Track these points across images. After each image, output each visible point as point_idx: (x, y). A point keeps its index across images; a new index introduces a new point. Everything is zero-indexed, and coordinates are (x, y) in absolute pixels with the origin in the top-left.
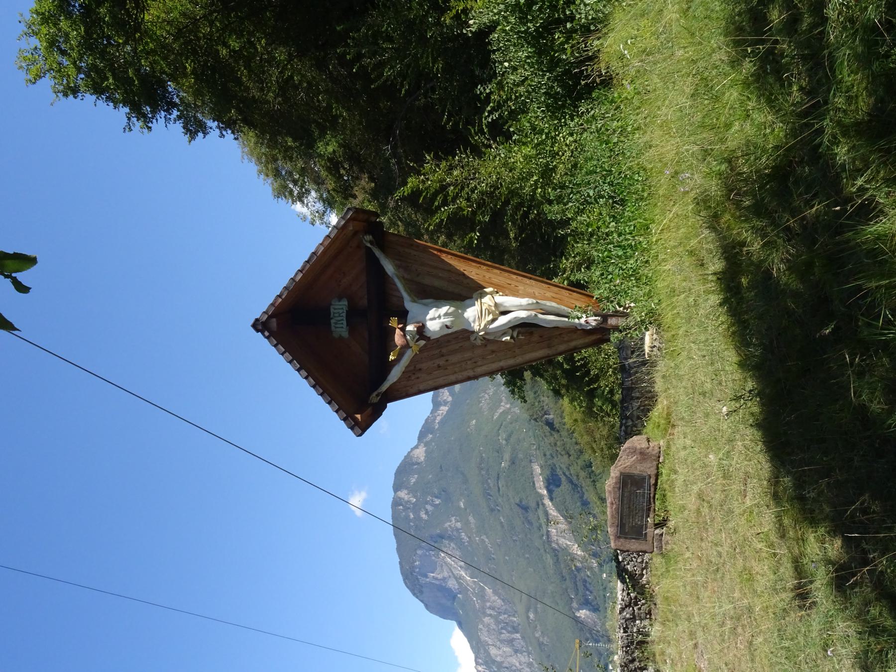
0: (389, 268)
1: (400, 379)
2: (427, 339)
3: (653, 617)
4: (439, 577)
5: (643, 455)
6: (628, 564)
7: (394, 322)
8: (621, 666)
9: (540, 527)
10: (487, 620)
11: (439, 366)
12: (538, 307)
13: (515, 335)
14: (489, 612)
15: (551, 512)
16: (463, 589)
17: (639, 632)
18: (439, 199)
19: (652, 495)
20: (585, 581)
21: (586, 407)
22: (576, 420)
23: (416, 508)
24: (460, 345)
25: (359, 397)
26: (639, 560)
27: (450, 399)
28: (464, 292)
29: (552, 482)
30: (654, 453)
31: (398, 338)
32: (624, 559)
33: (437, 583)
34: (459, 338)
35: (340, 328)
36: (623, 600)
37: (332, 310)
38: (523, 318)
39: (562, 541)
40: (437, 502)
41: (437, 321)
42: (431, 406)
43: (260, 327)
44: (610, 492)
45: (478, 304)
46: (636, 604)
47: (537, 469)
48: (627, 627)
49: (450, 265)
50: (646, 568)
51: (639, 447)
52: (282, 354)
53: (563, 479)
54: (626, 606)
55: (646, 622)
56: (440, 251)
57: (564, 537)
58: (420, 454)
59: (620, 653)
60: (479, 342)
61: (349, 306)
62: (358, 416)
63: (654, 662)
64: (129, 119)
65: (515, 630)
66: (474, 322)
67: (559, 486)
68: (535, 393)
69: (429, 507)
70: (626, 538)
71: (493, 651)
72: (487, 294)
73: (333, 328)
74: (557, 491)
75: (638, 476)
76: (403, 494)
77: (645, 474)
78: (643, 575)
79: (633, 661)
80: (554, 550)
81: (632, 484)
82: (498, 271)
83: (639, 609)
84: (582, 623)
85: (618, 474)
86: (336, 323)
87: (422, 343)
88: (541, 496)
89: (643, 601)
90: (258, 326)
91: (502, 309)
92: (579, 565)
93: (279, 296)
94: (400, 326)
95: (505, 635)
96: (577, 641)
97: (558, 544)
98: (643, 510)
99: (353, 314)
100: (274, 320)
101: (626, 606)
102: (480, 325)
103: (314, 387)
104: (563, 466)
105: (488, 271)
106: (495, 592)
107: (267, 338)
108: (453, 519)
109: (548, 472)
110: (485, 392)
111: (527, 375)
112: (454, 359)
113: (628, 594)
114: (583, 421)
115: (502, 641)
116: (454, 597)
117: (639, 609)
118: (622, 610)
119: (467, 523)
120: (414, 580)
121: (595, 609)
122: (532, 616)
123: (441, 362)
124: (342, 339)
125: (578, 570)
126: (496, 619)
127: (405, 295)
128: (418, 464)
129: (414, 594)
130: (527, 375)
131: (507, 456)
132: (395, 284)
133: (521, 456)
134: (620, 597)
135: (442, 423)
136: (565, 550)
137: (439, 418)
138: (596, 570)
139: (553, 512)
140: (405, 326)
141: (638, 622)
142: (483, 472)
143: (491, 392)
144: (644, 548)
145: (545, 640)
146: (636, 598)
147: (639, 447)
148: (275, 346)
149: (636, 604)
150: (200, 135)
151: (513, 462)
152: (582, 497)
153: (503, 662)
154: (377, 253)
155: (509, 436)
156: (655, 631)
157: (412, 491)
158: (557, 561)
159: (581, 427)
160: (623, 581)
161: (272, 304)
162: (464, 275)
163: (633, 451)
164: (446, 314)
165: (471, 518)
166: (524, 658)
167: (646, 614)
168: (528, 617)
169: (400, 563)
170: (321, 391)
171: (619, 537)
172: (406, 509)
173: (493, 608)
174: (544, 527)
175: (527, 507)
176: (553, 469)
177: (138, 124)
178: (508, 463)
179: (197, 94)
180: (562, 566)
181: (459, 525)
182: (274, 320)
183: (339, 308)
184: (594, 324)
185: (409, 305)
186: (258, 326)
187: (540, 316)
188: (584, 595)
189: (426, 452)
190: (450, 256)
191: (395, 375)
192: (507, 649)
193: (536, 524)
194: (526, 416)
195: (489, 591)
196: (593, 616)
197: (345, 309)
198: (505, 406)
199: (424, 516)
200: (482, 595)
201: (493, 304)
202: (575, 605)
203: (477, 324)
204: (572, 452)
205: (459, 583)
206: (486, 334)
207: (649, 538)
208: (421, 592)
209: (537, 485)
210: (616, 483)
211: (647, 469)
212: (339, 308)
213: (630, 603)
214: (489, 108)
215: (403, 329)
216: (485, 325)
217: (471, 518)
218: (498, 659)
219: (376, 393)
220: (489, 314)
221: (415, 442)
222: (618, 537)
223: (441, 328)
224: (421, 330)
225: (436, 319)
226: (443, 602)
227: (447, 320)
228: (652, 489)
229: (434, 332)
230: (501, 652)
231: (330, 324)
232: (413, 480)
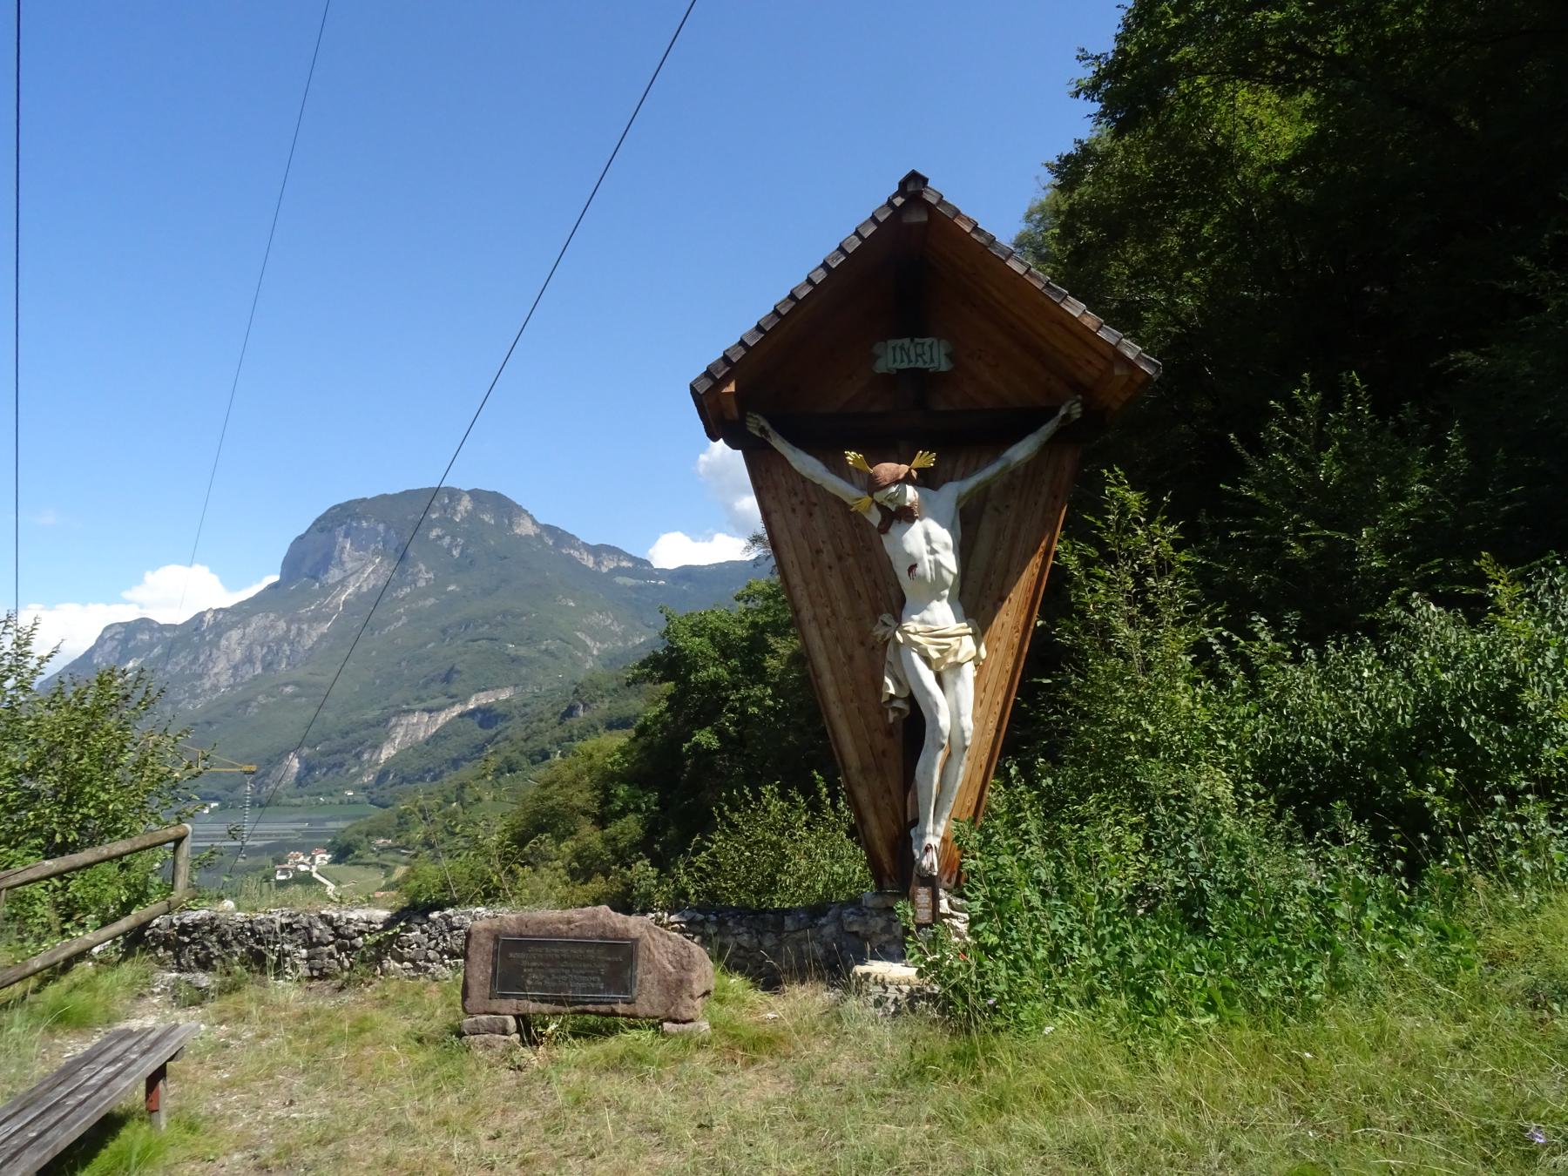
0: (1020, 452)
1: (798, 474)
2: (884, 528)
3: (315, 983)
4: (345, 557)
5: (677, 987)
6: (423, 932)
7: (924, 459)
8: (212, 919)
9: (420, 699)
10: (282, 625)
11: (819, 552)
12: (956, 749)
13: (898, 704)
14: (294, 628)
15: (443, 715)
16: (326, 590)
17: (283, 955)
18: (1092, 552)
19: (590, 1007)
20: (341, 765)
21: (613, 773)
22: (591, 757)
23: (446, 522)
25: (767, 397)
26: (431, 954)
27: (604, 570)
28: (976, 603)
29: (486, 716)
30: (682, 1009)
31: (887, 469)
32: (434, 922)
33: (336, 554)
34: (889, 594)
35: (894, 356)
36: (349, 921)
37: (928, 341)
38: (936, 721)
39: (400, 731)
40: (456, 553)
41: (925, 548)
42: (593, 542)
43: (910, 188)
44: (594, 917)
45: (963, 627)
46: (340, 949)
47: (504, 695)
48: (293, 931)
49: (1020, 573)
50: (417, 968)
51: (694, 976)
52: (857, 233)
53: (492, 732)
54: (336, 929)
55: (304, 970)
57: (405, 735)
58: (525, 528)
59: (240, 916)
61: (938, 375)
62: (731, 388)
63: (222, 991)
64: (1097, 58)
65: (268, 666)
66: (923, 621)
67: (481, 725)
68: (615, 690)
69: (447, 540)
70: (495, 953)
71: (235, 635)
72: (978, 646)
73: (891, 343)
74: (472, 724)
75: (632, 978)
76: (466, 504)
77: (635, 991)
78: (401, 962)
79: (225, 944)
80: (387, 720)
81: (611, 963)
82: (1009, 666)
83: (331, 956)
84: (280, 762)
85: (634, 934)
86: (902, 348)
87: (875, 518)
88: (465, 701)
89: (347, 963)
90: (913, 185)
91: (948, 677)
92: (366, 756)
93: (975, 228)
94: (914, 474)
95: (259, 652)
96: (254, 768)
97: (395, 726)
98: (561, 989)
99: (919, 378)
100: (925, 218)
101: (336, 929)
102: (916, 633)
103: (792, 296)
104: (510, 731)
105: (1009, 646)
106: (323, 636)
107: (890, 203)
108: (431, 575)
109: (500, 710)
110: (616, 618)
111: (669, 687)
112: (835, 583)
113: (361, 933)
114: (590, 769)
115: (250, 647)
116: (315, 578)
117: (331, 956)
118: (329, 921)
119: (424, 594)
120: (340, 518)
121: (300, 781)
122: (289, 689)
123: (827, 557)
124: (858, 364)
125: (358, 756)
126: (284, 638)
127: (972, 482)
128: (511, 524)
129: (318, 520)
130: (669, 687)
131: (523, 651)
132: (988, 464)
133: (524, 671)
134: (354, 916)
135: (570, 557)
136: (388, 737)
137: (576, 554)
138: (358, 782)
139: (442, 718)
140: (914, 483)
141: (304, 952)
142: (499, 618)
143: (616, 628)
144: (475, 992)
145: (253, 710)
146: (354, 948)
147: (694, 976)
148: (873, 219)
149: (340, 949)
150: (1058, 182)
151: (515, 660)
152: (465, 759)
153: (218, 649)
154: (1048, 429)
155: (552, 654)
156: (287, 991)
157: (471, 516)
158: (369, 725)
159: (582, 766)
160: (389, 923)
161: (957, 213)
162: (1002, 599)
163: (685, 965)
164: (938, 565)
165: (432, 601)
166: (225, 679)
167: (321, 970)
168: (286, 685)
169: (364, 500)
170: (784, 311)
171: (496, 939)
172: (444, 508)
173: (300, 632)
174: (423, 705)
175: (448, 681)
176: (505, 717)
177: (1087, 73)
178: (513, 653)
179: (1126, 178)
180: (364, 733)
181: (422, 584)
182: (925, 218)
183: (933, 355)
184: (925, 863)
185: (951, 492)
186: (913, 185)
187: (941, 755)
188: (320, 766)
189: (528, 536)
190: (1036, 571)
191: (806, 464)
192: (238, 655)
193: (424, 694)
194: (581, 678)
195: (325, 628)
196: (290, 779)
197: (932, 367)
198: (595, 648)
199: (434, 533)
200: (318, 618)
201: (960, 658)
202: (306, 751)
203: (920, 628)
204: (530, 744)
205: (334, 586)
206: (897, 643)
207: (496, 1004)
208: (322, 530)
209: (481, 695)
210: (614, 930)
211: (648, 999)
212: (933, 355)
213: (343, 937)
214: (1235, 638)
215: (908, 479)
216: (917, 644)
217: (432, 601)
218: (223, 642)
219: (768, 427)
220: (940, 651)
221: (542, 521)
222: (496, 936)
223: (910, 555)
224: (907, 515)
225: (929, 543)
226: (308, 560)
227: (926, 567)
228: (603, 1008)
229: (900, 543)
230: (233, 646)
231: (900, 335)
232: (486, 518)
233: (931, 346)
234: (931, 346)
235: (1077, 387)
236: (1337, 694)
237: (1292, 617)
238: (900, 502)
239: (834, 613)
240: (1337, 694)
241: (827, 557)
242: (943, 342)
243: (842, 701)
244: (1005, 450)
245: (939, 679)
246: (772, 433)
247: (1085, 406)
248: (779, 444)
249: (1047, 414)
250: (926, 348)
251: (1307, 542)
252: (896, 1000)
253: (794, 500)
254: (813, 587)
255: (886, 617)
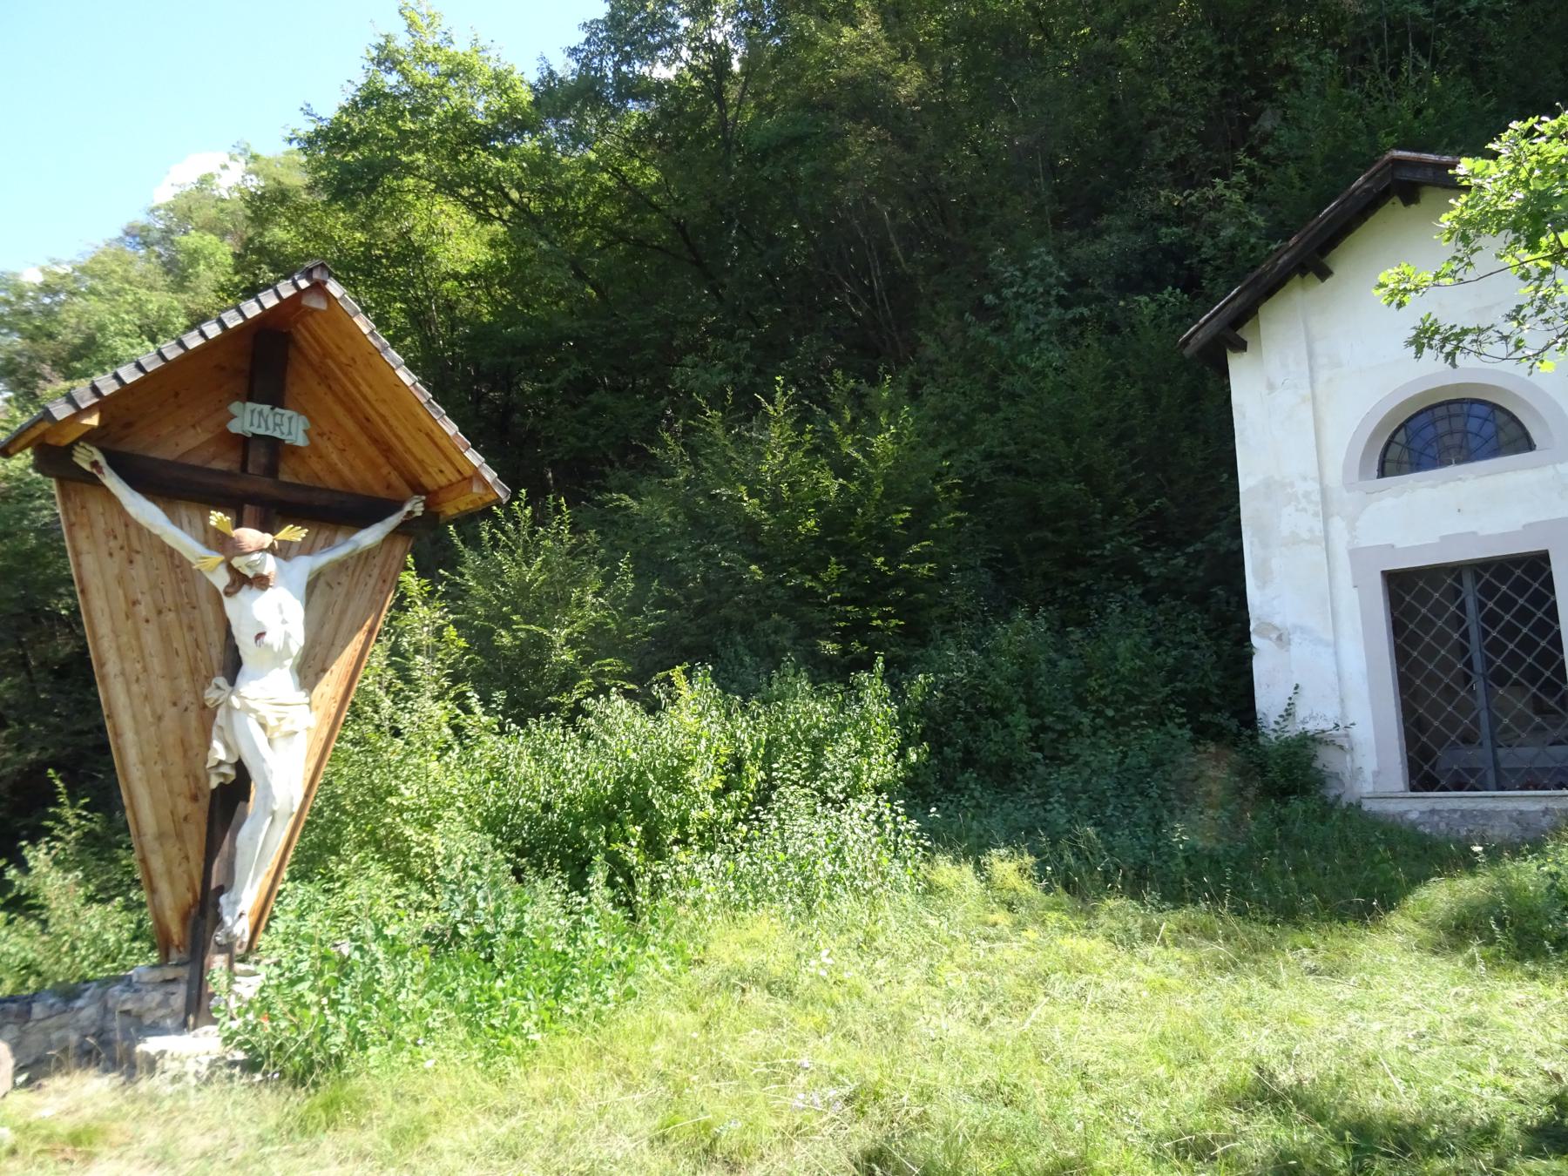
0: (369, 537)
24: (182, 651)
35: (250, 419)
37: (288, 413)
49: (344, 647)
56: (371, 631)
60: (211, 695)
61: (294, 450)
73: (250, 405)
86: (261, 413)
87: (221, 580)
99: (274, 446)
112: (150, 638)
154: (394, 521)
162: (324, 670)
185: (304, 566)
190: (359, 647)
197: (289, 440)
212: (291, 427)
215: (271, 549)
225: (275, 615)
233: (290, 419)
234: (290, 419)
235: (417, 488)
236: (553, 766)
237: (499, 696)
238: (259, 569)
239: (145, 669)
240: (553, 766)
241: (143, 610)
242: (303, 418)
243: (143, 763)
244: (354, 533)
245: (270, 741)
246: (107, 470)
247: (426, 505)
248: (112, 482)
249: (393, 506)
250: (285, 420)
251: (514, 633)
252: (197, 1072)
253: (112, 543)
254: (124, 639)
255: (221, 681)
